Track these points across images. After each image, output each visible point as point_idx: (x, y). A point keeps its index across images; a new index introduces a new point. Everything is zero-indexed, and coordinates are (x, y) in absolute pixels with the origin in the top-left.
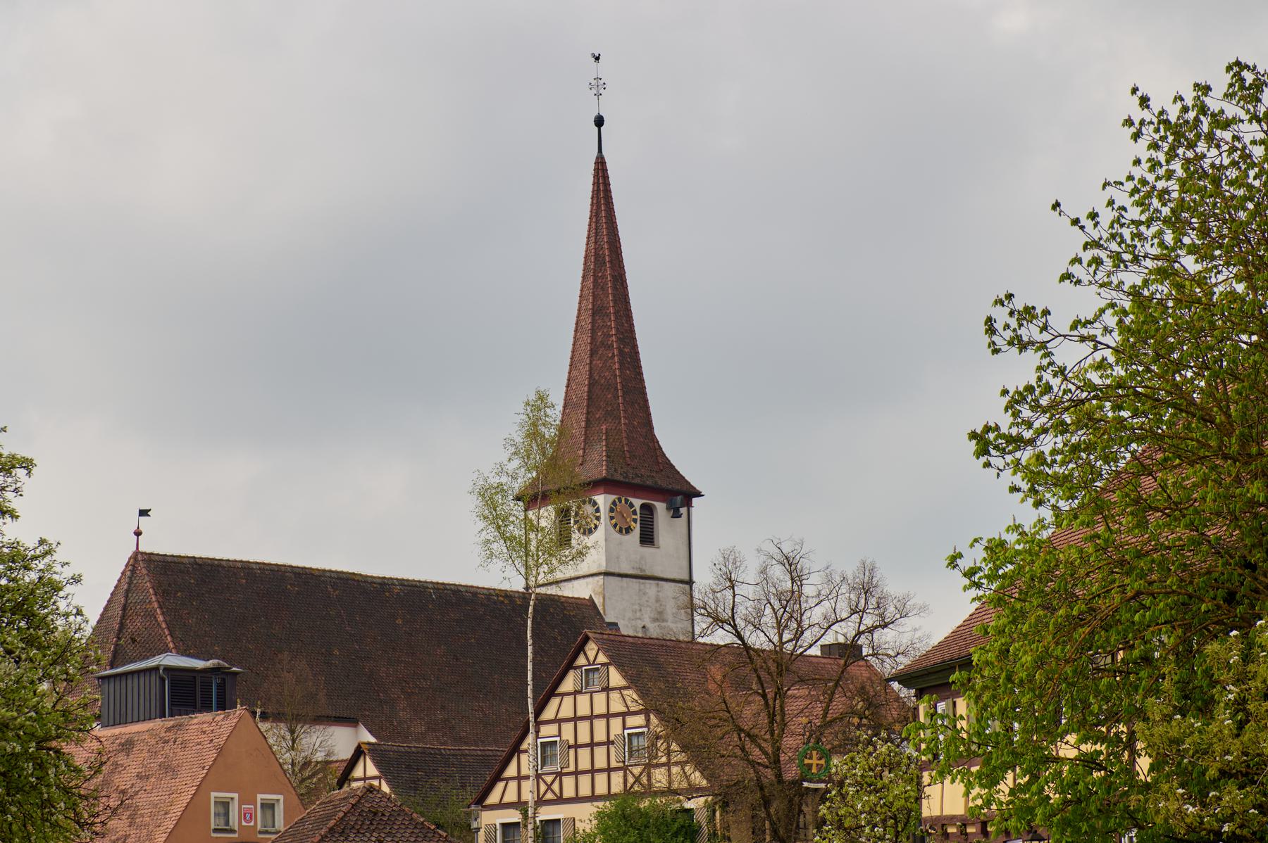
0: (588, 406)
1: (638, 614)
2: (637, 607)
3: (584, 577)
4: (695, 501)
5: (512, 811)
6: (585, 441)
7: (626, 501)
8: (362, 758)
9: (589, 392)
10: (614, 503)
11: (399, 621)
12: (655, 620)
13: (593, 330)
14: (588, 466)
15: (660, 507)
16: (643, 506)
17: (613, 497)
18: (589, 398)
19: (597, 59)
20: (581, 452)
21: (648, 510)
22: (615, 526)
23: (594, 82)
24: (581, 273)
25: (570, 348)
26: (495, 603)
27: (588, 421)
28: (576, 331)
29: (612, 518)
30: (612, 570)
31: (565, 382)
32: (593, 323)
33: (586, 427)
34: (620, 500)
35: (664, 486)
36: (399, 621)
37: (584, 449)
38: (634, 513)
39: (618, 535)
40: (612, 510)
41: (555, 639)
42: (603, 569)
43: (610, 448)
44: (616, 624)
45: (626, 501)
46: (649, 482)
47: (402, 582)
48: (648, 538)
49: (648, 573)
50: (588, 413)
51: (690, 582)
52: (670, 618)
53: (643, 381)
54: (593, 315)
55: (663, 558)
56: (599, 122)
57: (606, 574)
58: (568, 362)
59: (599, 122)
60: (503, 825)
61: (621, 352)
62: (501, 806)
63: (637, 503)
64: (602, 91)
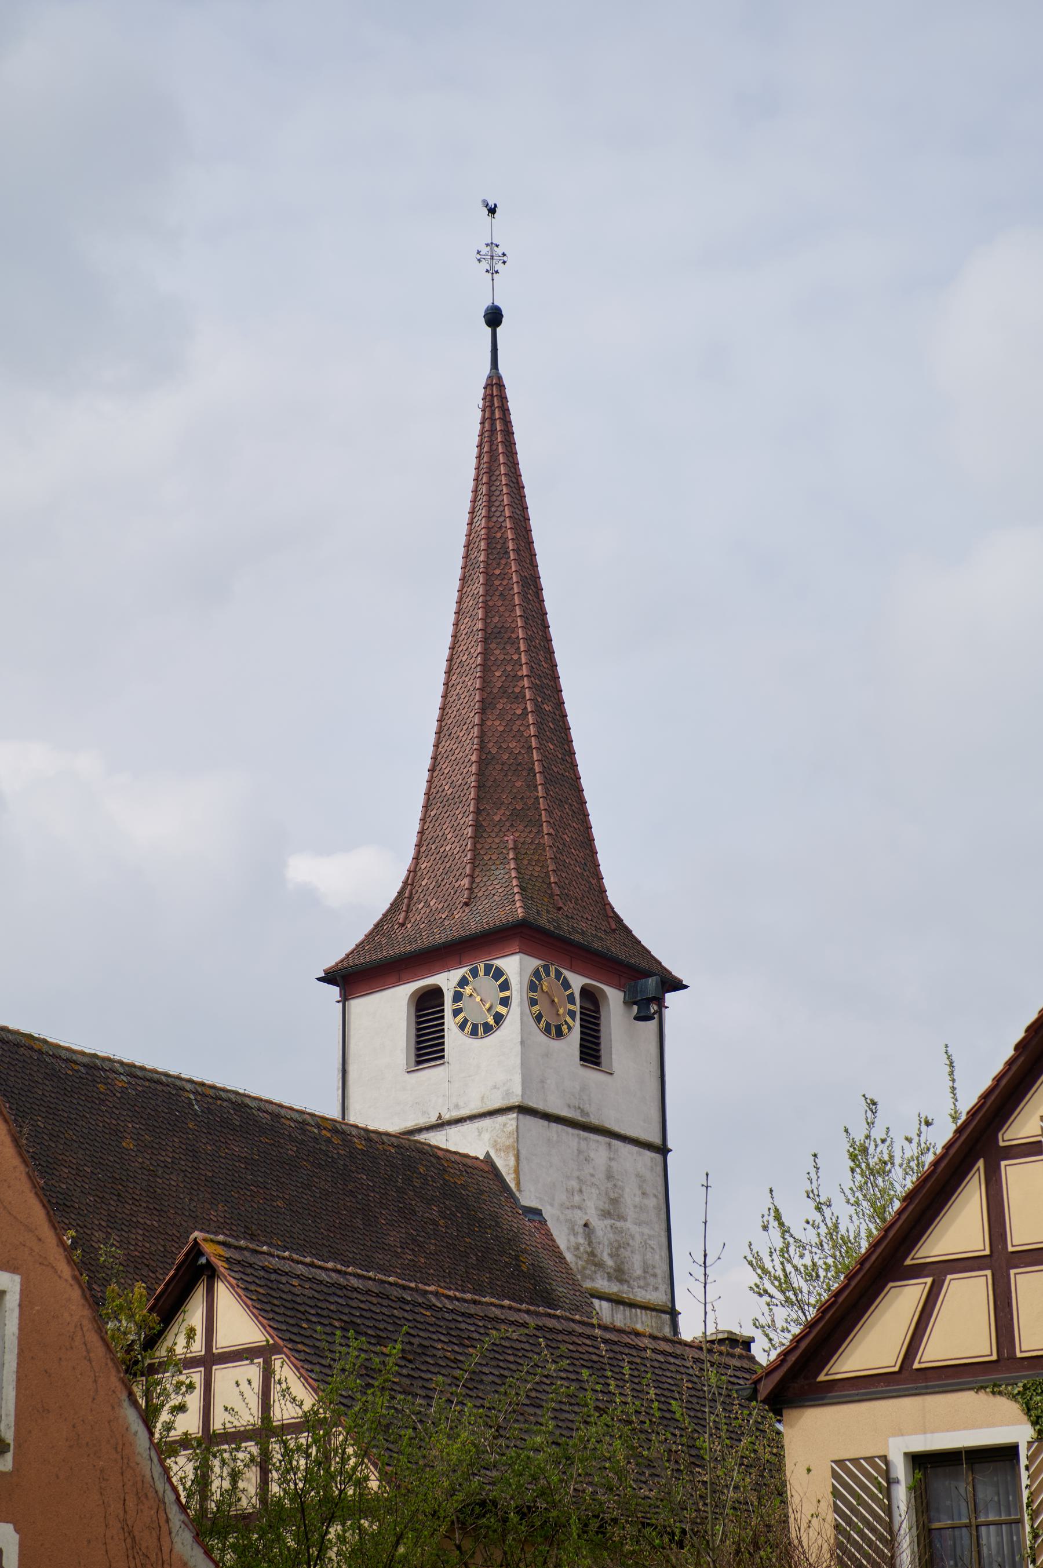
0: (478, 799)
1: (577, 1198)
2: (574, 1184)
3: (472, 1118)
4: (670, 998)
5: (967, 1401)
6: (473, 862)
7: (558, 974)
8: (199, 1296)
9: (480, 774)
10: (536, 973)
11: (128, 1144)
12: (606, 1214)
13: (485, 667)
14: (482, 905)
15: (614, 997)
16: (585, 991)
17: (534, 963)
18: (479, 787)
19: (492, 211)
20: (466, 882)
21: (591, 998)
22: (538, 1018)
23: (485, 250)
24: (458, 573)
25: (438, 701)
26: (315, 1139)
27: (477, 826)
28: (449, 672)
29: (533, 1002)
30: (533, 1104)
31: (428, 763)
32: (486, 653)
33: (476, 837)
34: (546, 969)
35: (623, 957)
36: (128, 1144)
37: (472, 876)
38: (571, 999)
39: (543, 1038)
40: (532, 987)
41: (435, 1223)
42: (515, 1100)
43: (516, 879)
44: (538, 1212)
45: (558, 974)
46: (596, 945)
47: (132, 1071)
48: (591, 1053)
49: (594, 1120)
50: (478, 812)
51: (663, 1150)
52: (631, 1213)
53: (574, 765)
54: (485, 641)
55: (615, 1095)
56: (494, 318)
57: (523, 1110)
58: (434, 726)
59: (494, 318)
60: (918, 1461)
61: (538, 710)
62: (910, 1378)
63: (577, 982)
64: (499, 266)
